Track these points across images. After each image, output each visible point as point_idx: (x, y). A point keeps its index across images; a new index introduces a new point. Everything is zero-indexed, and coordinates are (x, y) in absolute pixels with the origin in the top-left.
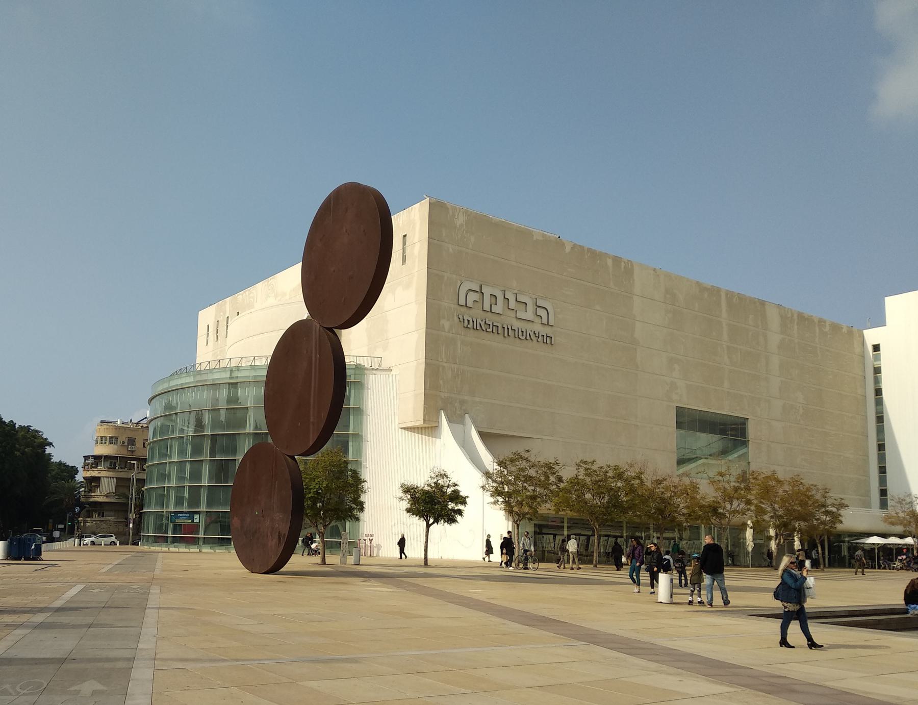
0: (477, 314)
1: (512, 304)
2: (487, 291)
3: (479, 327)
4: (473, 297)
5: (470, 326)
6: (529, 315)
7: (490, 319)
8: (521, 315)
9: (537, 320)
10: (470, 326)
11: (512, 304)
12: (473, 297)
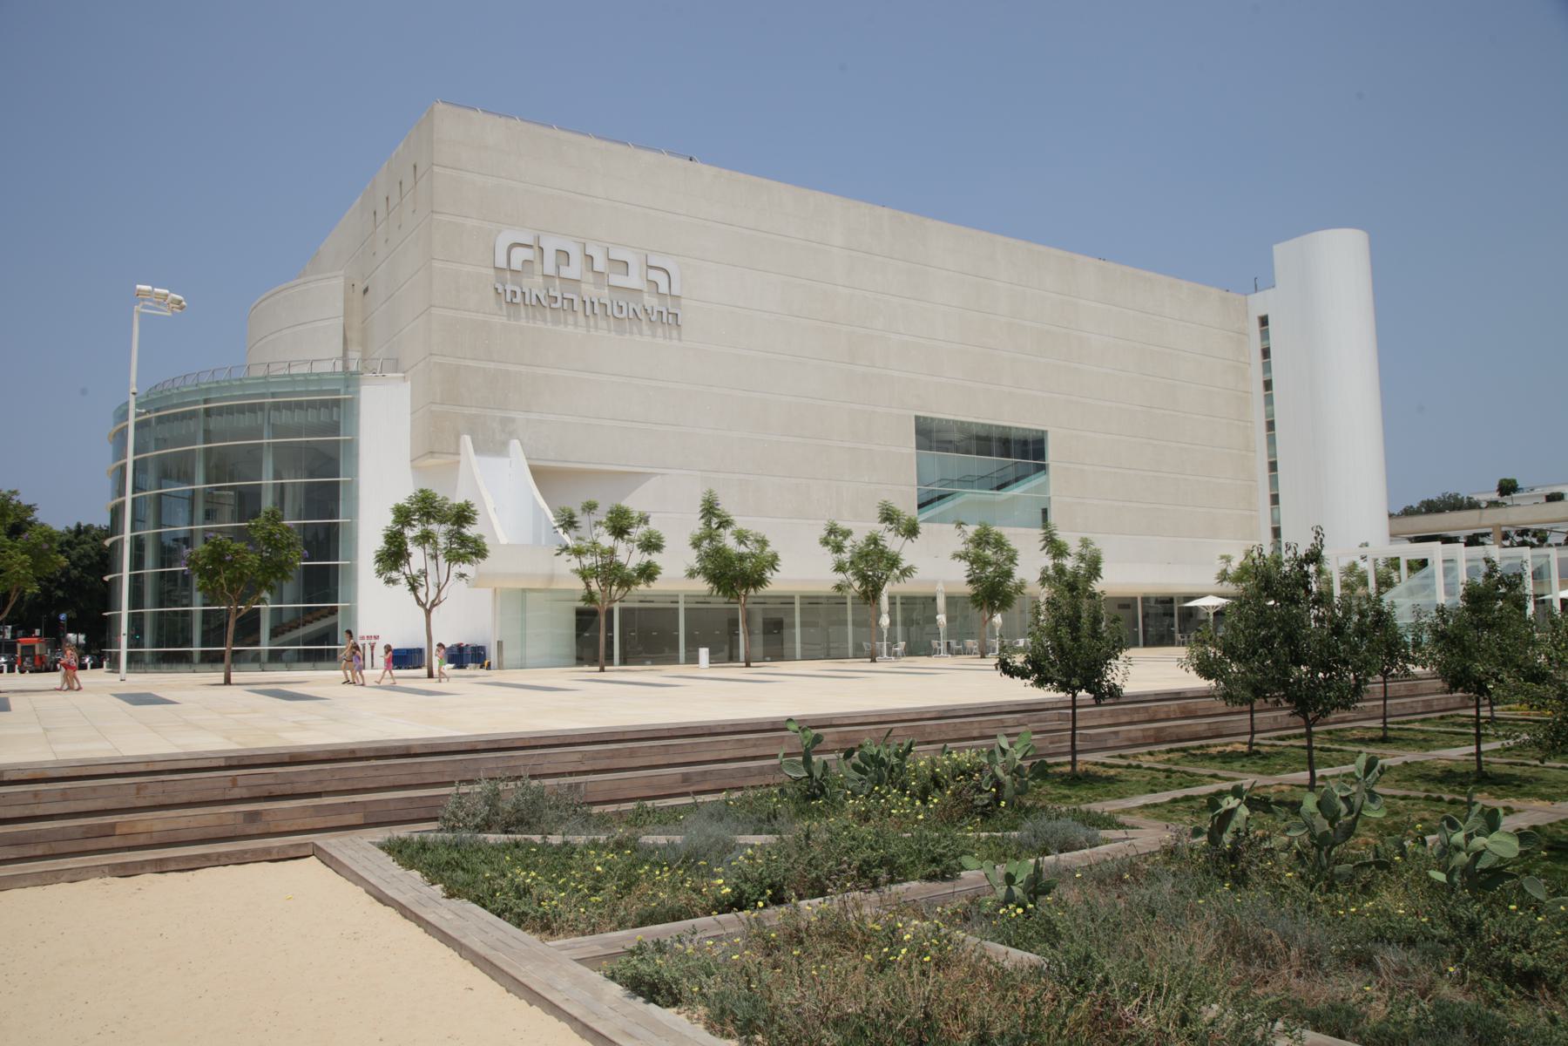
0: (534, 285)
1: (600, 264)
2: (550, 245)
3: (534, 301)
4: (519, 255)
5: (518, 299)
6: (634, 280)
8: (617, 280)
10: (518, 299)
12: (519, 255)
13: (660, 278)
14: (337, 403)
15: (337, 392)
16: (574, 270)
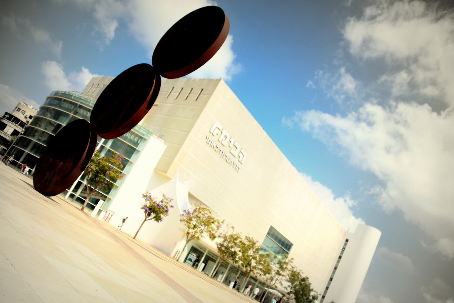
2: (225, 133)
6: (236, 153)
7: (219, 146)
9: (237, 157)
11: (231, 145)
13: (241, 155)
14: (141, 138)
15: (144, 135)
16: (226, 143)
